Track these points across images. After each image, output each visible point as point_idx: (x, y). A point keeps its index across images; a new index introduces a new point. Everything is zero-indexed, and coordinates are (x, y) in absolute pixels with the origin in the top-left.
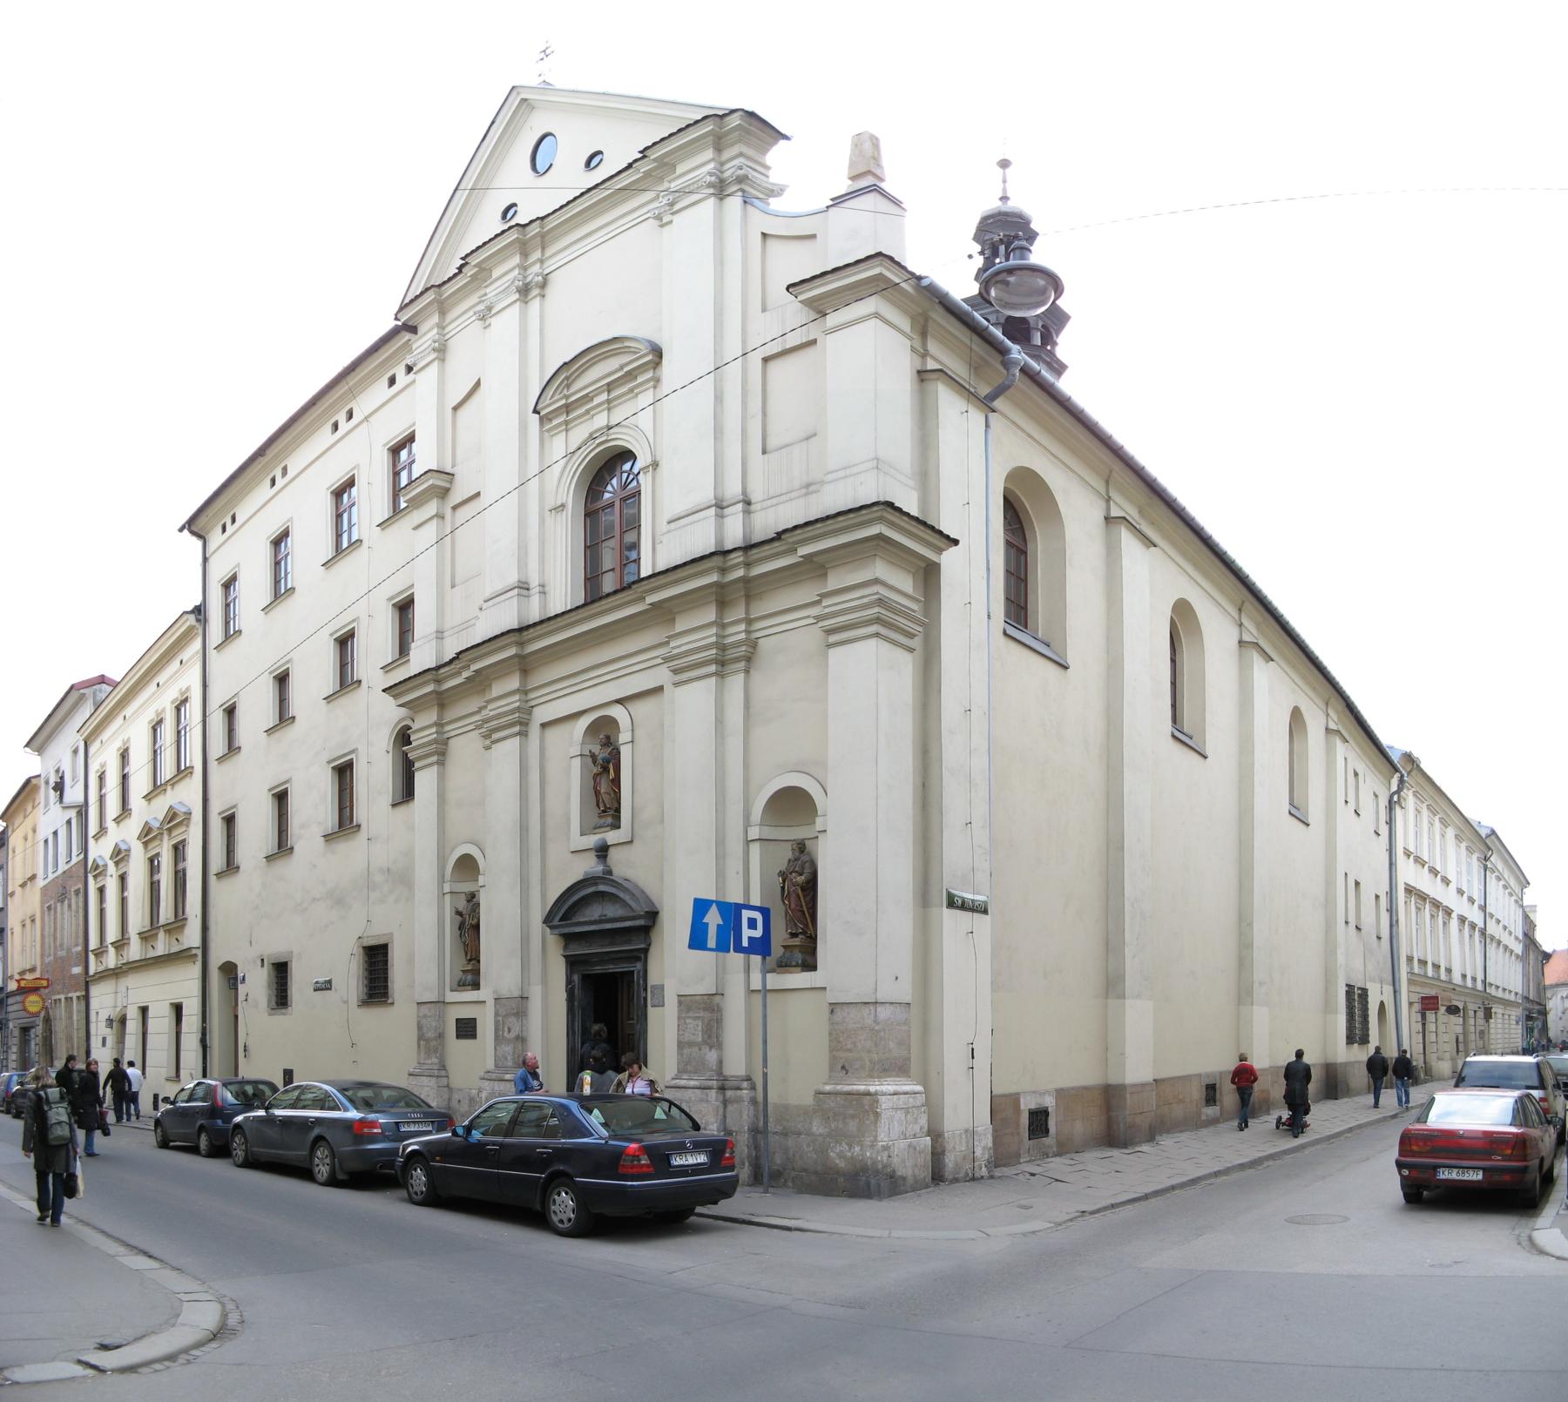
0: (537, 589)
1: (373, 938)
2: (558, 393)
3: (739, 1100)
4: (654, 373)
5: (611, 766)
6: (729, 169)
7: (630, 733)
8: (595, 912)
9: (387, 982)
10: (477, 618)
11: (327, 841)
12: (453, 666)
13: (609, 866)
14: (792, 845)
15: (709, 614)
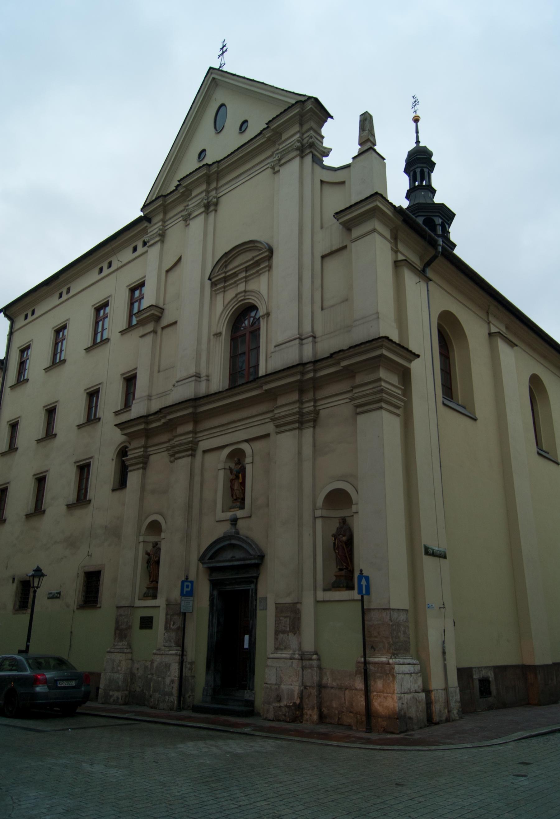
0: (205, 378)
1: (92, 565)
2: (221, 270)
3: (311, 667)
4: (269, 262)
5: (240, 475)
6: (306, 138)
7: (252, 457)
8: (228, 555)
9: (98, 594)
10: (171, 390)
11: (87, 352)
12: (156, 416)
13: (237, 530)
14: (339, 520)
15: (295, 397)
